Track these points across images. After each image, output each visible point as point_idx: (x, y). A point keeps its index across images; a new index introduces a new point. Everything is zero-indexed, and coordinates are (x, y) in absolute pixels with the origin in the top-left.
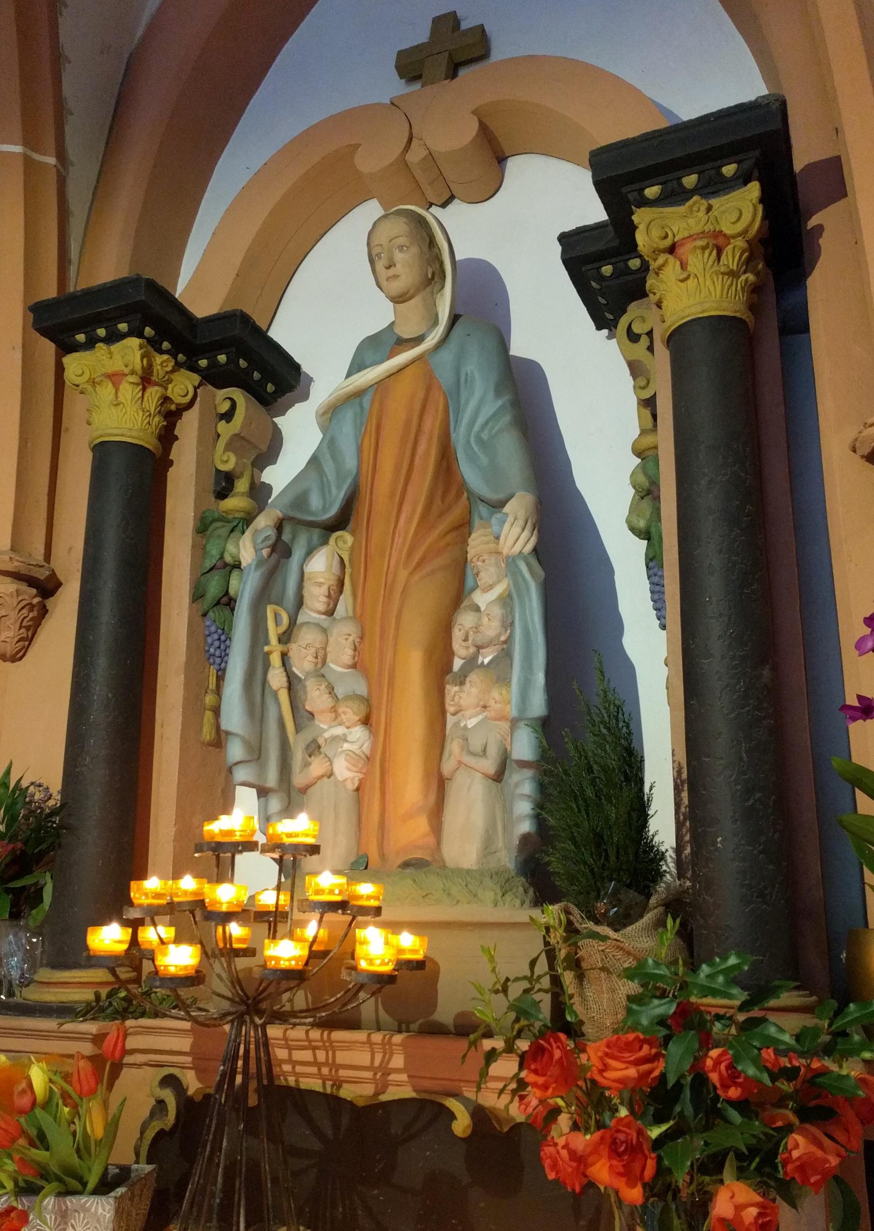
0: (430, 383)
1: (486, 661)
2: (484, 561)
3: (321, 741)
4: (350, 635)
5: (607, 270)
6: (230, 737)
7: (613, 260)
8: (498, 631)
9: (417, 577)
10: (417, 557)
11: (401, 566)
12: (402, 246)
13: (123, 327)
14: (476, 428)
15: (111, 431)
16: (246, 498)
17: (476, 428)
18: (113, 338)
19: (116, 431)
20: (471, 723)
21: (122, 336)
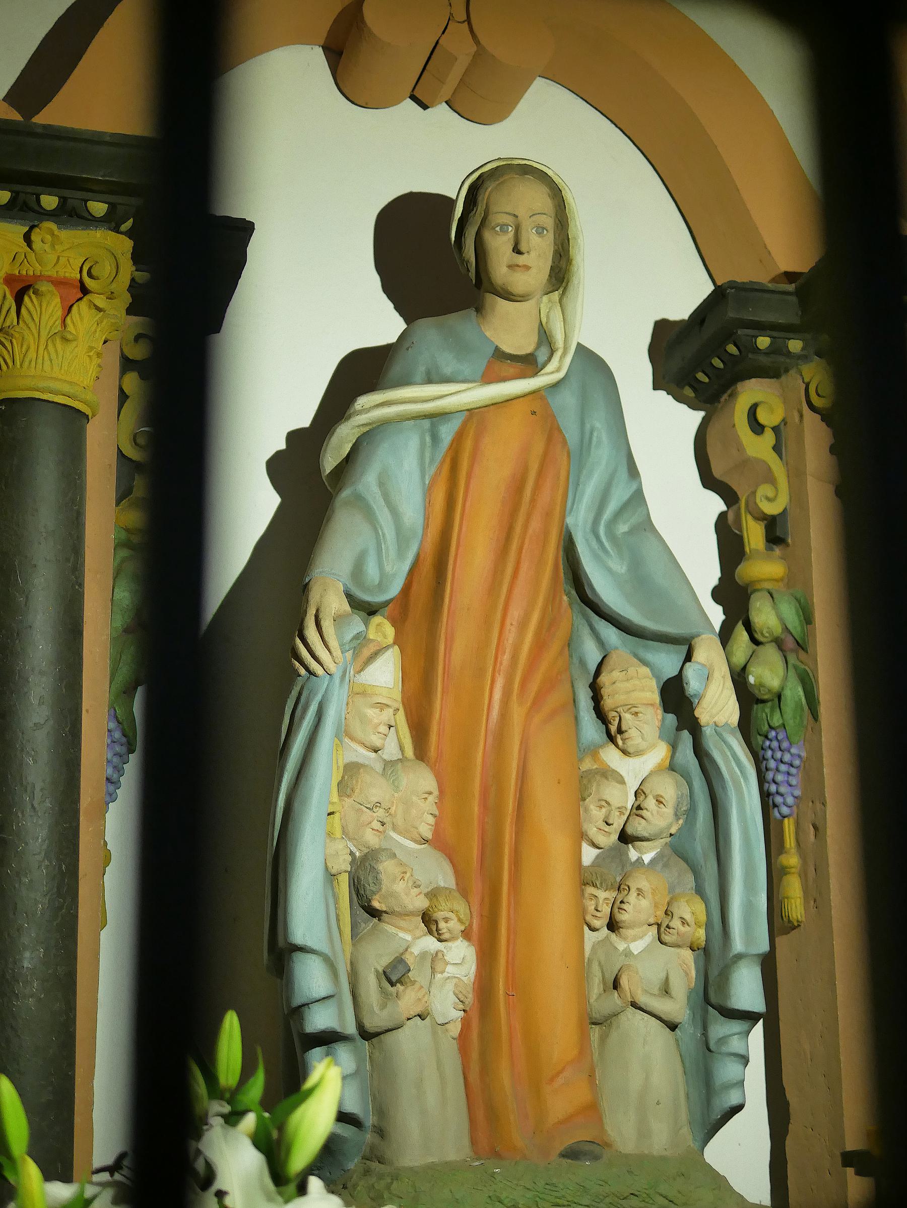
0: (552, 432)
1: (647, 858)
2: (636, 714)
3: (410, 960)
4: (430, 793)
5: (763, 342)
6: (298, 957)
7: (775, 334)
8: (670, 821)
9: (537, 719)
10: (534, 687)
11: (514, 697)
12: (543, 228)
13: (98, 208)
14: (607, 515)
15: (53, 385)
16: (692, 694)
17: (607, 515)
18: (71, 215)
19: (66, 388)
20: (637, 947)
21: (90, 221)
